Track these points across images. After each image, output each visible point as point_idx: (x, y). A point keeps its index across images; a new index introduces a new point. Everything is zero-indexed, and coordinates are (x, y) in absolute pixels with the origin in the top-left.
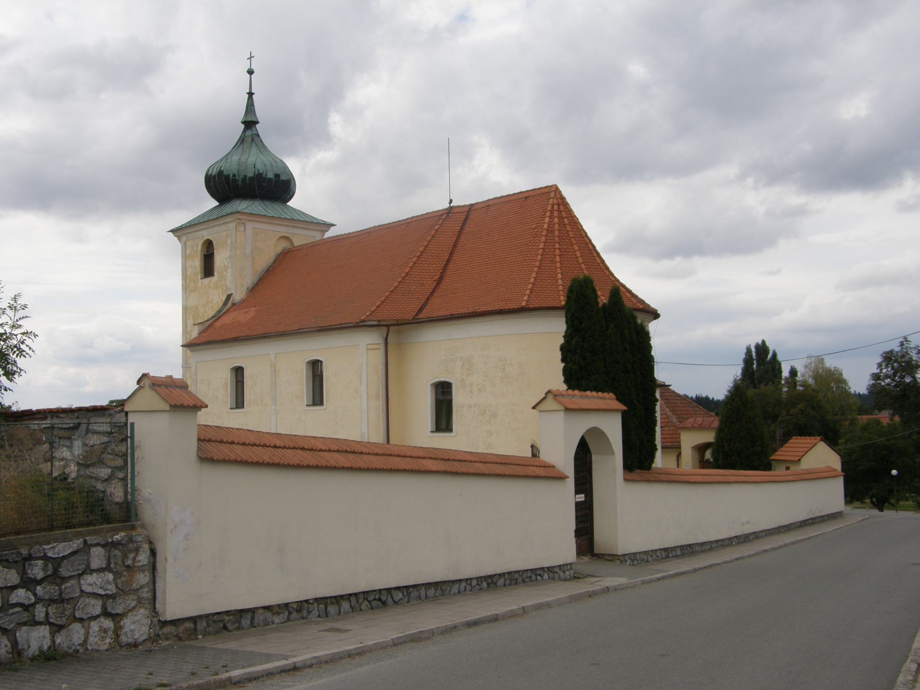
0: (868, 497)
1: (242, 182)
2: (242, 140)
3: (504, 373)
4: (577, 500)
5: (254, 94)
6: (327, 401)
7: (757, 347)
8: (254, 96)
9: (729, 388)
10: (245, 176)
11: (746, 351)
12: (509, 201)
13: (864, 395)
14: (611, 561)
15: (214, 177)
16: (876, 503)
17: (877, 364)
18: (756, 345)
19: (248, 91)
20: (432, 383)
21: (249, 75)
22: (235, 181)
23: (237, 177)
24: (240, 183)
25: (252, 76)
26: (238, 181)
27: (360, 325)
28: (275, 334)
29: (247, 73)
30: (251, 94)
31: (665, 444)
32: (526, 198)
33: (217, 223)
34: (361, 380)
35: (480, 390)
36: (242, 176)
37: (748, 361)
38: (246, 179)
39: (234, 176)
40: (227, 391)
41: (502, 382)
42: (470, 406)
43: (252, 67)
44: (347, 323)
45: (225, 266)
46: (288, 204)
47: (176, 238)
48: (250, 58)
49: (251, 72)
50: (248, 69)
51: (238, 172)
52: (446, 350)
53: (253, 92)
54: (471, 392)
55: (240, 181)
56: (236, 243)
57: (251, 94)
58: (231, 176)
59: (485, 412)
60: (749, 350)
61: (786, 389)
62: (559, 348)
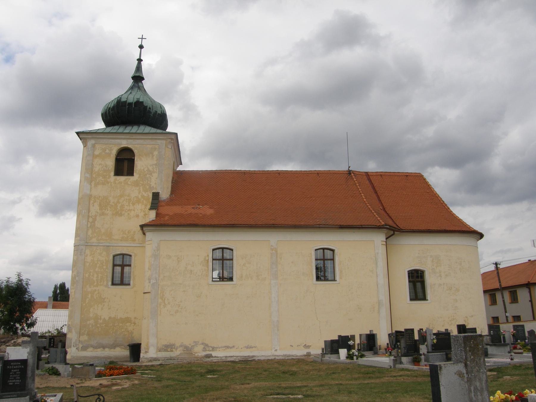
0: (515, 333)
1: (153, 115)
2: (132, 88)
3: (461, 266)
4: (407, 343)
5: (142, 60)
7: (61, 285)
8: (142, 62)
10: (156, 112)
11: (54, 287)
12: (402, 176)
15: (130, 104)
19: (138, 58)
20: (408, 270)
22: (150, 112)
23: (151, 110)
24: (152, 115)
25: (142, 50)
26: (151, 113)
27: (378, 228)
28: (292, 226)
32: (407, 176)
33: (148, 137)
34: (377, 264)
35: (447, 275)
36: (154, 111)
37: (55, 292)
38: (156, 113)
39: (150, 108)
40: (208, 267)
41: (461, 271)
42: (440, 285)
43: (142, 44)
44: (370, 225)
45: (148, 170)
48: (142, 38)
49: (141, 47)
51: (152, 106)
52: (419, 251)
54: (440, 276)
55: (153, 113)
56: (165, 156)
58: (148, 108)
59: (452, 288)
60: (56, 286)
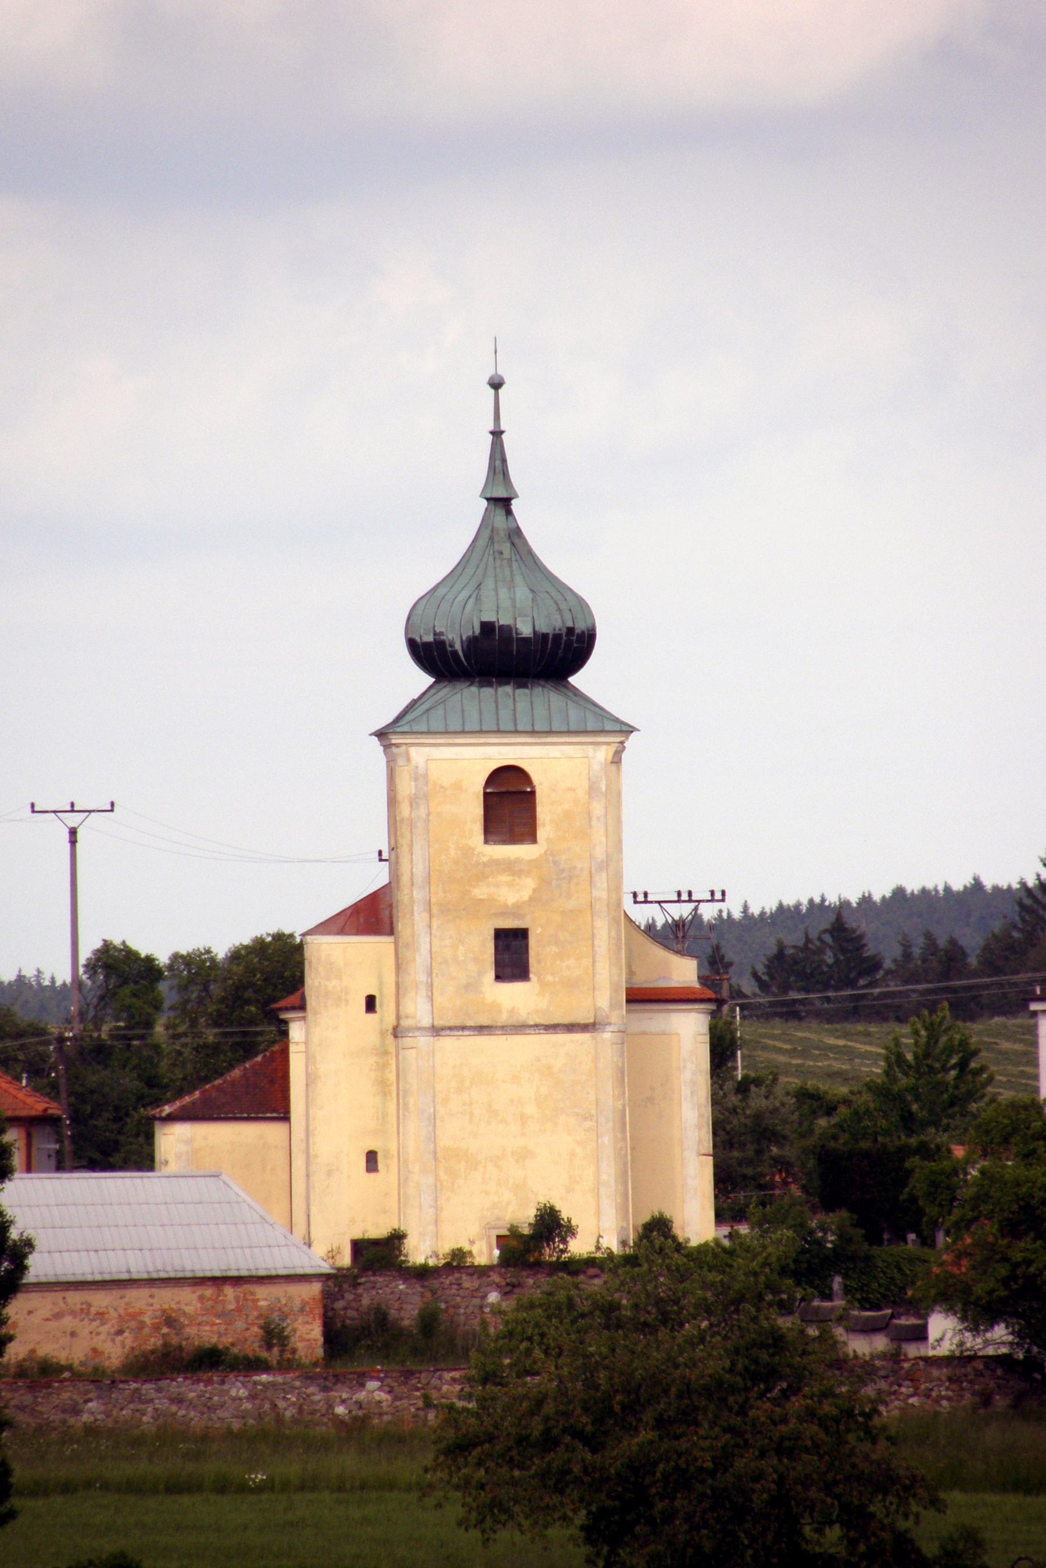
5: (502, 432)
6: (381, 1006)
8: (504, 436)
9: (29, 973)
13: (875, 903)
14: (382, 1084)
16: (110, 987)
17: (105, 941)
18: (259, 947)
19: (491, 427)
21: (492, 391)
25: (500, 391)
29: (488, 387)
30: (497, 434)
31: (301, 1015)
46: (573, 680)
47: (382, 748)
49: (496, 385)
50: (491, 378)
53: (502, 428)
57: (497, 434)
61: (538, 932)
62: (172, 952)
